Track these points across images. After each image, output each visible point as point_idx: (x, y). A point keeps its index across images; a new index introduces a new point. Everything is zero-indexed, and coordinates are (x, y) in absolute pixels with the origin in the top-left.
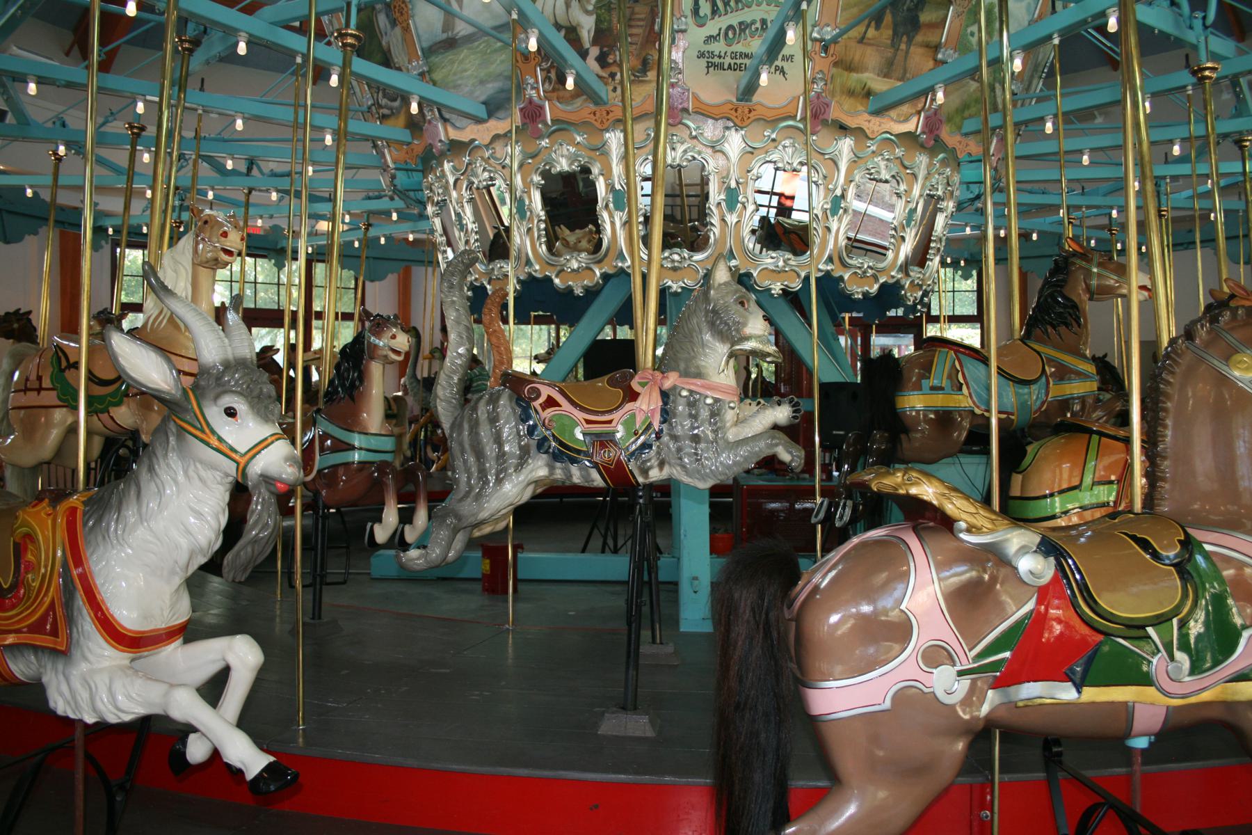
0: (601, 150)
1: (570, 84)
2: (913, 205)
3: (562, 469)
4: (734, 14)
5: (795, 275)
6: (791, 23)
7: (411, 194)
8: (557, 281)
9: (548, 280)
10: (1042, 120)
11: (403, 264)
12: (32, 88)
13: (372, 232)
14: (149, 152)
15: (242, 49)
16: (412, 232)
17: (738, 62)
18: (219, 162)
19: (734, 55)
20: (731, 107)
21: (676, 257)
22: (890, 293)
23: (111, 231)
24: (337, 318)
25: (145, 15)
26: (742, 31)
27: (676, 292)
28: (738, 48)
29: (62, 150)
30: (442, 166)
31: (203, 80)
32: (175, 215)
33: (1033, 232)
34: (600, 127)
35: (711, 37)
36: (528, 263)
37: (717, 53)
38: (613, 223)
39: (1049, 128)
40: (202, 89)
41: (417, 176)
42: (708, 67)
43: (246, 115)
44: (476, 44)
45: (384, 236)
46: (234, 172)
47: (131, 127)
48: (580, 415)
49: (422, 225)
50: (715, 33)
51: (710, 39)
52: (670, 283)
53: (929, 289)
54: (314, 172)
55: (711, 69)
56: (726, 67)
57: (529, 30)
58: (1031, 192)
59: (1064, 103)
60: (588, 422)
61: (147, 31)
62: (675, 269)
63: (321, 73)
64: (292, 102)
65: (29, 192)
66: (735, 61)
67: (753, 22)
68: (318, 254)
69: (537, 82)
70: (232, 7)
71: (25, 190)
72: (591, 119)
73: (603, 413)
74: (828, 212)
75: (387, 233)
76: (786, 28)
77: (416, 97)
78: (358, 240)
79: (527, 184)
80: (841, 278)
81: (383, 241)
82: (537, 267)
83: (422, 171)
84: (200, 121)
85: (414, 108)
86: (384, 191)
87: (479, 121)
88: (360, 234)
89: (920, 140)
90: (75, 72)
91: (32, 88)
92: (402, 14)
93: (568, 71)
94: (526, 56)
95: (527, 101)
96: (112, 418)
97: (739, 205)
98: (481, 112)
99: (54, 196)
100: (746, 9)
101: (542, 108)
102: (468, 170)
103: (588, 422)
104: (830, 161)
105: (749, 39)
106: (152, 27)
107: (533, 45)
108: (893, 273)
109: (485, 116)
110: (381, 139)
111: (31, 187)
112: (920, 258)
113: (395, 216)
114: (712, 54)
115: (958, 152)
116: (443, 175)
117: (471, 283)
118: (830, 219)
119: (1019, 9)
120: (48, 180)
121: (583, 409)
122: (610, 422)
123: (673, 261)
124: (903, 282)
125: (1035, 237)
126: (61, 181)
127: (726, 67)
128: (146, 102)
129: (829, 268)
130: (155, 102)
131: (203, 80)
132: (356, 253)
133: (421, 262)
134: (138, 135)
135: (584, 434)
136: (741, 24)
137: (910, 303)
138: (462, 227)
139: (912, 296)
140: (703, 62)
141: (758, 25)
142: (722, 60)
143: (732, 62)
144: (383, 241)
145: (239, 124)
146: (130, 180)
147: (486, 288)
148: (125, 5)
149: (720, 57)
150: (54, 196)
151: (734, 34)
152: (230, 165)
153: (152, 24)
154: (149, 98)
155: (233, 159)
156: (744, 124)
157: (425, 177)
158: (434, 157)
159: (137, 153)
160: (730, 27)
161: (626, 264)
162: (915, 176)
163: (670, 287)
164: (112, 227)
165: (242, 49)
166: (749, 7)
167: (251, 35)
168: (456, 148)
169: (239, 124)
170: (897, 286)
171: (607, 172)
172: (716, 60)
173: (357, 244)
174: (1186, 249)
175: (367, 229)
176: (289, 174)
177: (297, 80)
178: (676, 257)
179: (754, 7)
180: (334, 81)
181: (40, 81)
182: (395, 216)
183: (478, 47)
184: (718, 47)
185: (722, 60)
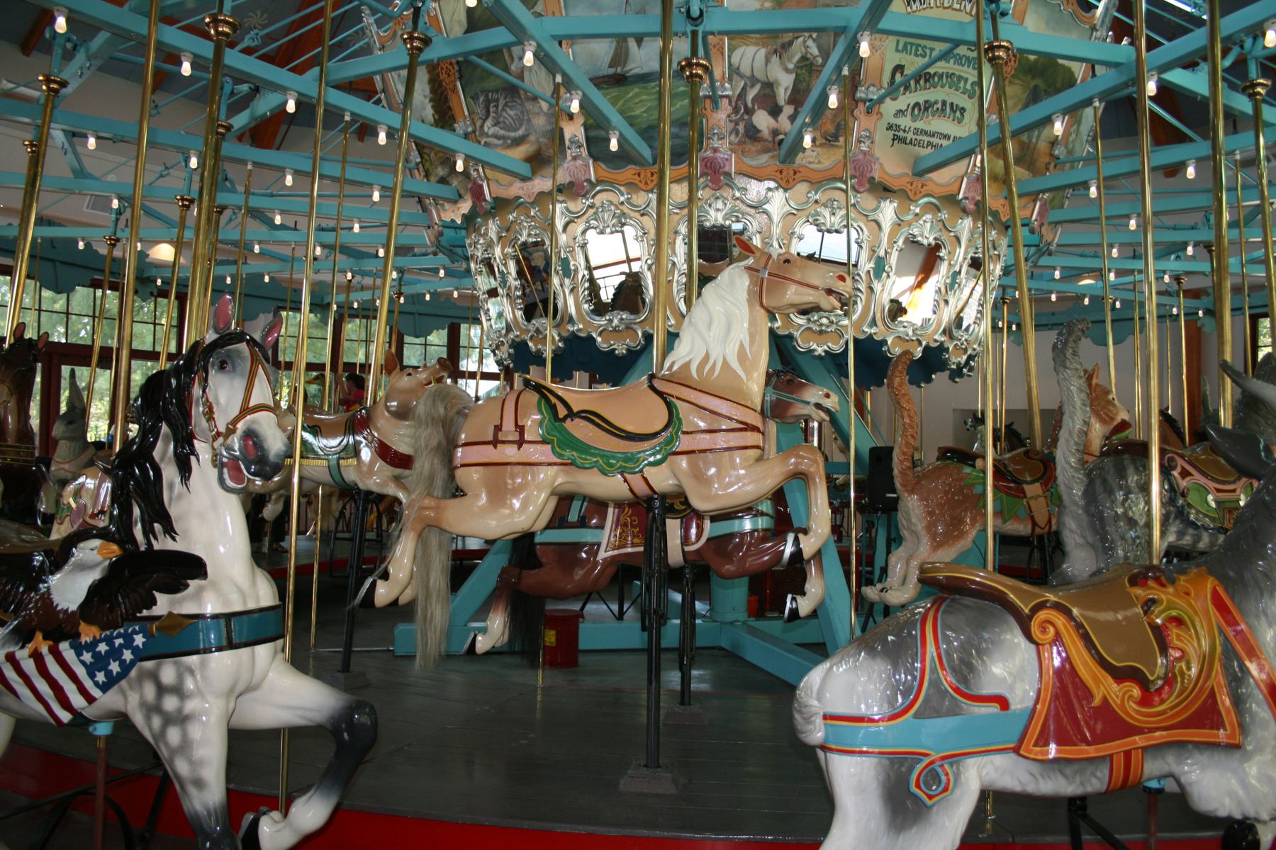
2: (957, 268)
3: (1192, 535)
4: (922, 92)
10: (1085, 185)
12: (92, 142)
17: (919, 138)
19: (916, 132)
21: (824, 321)
23: (159, 282)
25: (198, 74)
26: (926, 109)
27: (820, 355)
28: (920, 125)
30: (487, 224)
35: (900, 111)
36: (571, 320)
37: (902, 127)
38: (961, 266)
39: (1093, 191)
41: (463, 232)
42: (894, 140)
48: (1212, 485)
49: (466, 282)
50: (904, 108)
51: (900, 113)
52: (815, 346)
53: (974, 353)
55: (896, 142)
56: (908, 141)
58: (1081, 256)
59: (1109, 169)
60: (1218, 491)
62: (821, 332)
63: (366, 130)
64: (340, 158)
65: (81, 245)
66: (915, 137)
67: (936, 102)
68: (363, 309)
73: (1229, 483)
76: (828, 92)
80: (884, 342)
81: (428, 297)
84: (250, 176)
85: (460, 166)
86: (426, 246)
87: (524, 179)
89: (962, 205)
91: (92, 142)
96: (645, 479)
97: (885, 274)
98: (525, 169)
100: (932, 89)
103: (1218, 491)
104: (874, 224)
105: (930, 117)
109: (530, 175)
110: (428, 197)
114: (898, 127)
115: (1002, 215)
117: (513, 340)
119: (228, 5)
121: (1214, 480)
122: (1234, 491)
123: (822, 325)
124: (946, 345)
125: (1086, 301)
127: (908, 141)
129: (873, 331)
135: (1217, 502)
136: (926, 102)
140: (891, 133)
141: (939, 106)
142: (905, 135)
143: (914, 137)
144: (428, 297)
145: (289, 180)
147: (594, 340)
148: (180, 65)
149: (904, 131)
151: (920, 110)
160: (917, 104)
161: (776, 325)
162: (958, 240)
163: (814, 350)
164: (162, 278)
166: (935, 87)
167: (300, 94)
168: (501, 205)
169: (289, 180)
170: (942, 348)
172: (901, 134)
174: (1050, 329)
176: (333, 230)
177: (345, 138)
178: (824, 321)
179: (939, 88)
182: (442, 273)
184: (904, 122)
185: (905, 135)
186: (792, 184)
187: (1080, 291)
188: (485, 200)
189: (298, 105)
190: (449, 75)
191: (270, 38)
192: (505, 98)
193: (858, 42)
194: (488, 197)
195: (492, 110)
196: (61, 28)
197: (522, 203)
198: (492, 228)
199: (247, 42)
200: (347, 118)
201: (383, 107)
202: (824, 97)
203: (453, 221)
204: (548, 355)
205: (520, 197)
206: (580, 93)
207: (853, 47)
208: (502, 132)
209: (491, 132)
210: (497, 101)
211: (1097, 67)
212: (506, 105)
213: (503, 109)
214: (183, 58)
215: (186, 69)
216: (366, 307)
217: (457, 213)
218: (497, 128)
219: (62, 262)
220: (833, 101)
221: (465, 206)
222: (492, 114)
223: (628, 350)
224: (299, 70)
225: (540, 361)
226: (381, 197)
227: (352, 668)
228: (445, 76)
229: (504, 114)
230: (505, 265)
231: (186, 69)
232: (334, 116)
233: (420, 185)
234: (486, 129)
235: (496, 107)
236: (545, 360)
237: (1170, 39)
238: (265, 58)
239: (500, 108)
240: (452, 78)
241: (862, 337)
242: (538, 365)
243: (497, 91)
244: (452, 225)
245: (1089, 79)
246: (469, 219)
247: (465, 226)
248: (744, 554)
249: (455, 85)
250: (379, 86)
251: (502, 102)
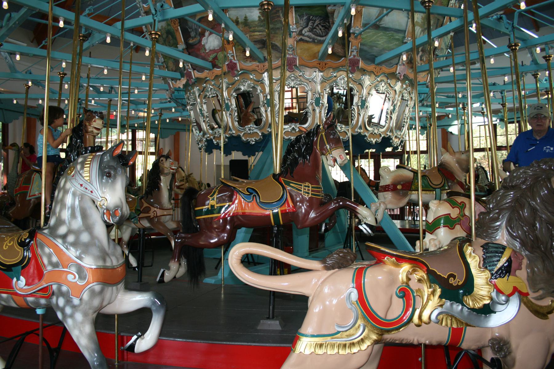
0: (261, 82)
1: (248, 54)
5: (345, 133)
6: (354, 5)
7: (179, 101)
8: (243, 138)
9: (239, 137)
11: (176, 131)
12: (18, 57)
13: (163, 117)
14: (68, 84)
15: (108, 40)
16: (181, 117)
18: (97, 88)
20: (318, 62)
22: (387, 141)
24: (144, 152)
25: (67, 26)
29: (30, 84)
31: (90, 52)
32: (78, 111)
33: (450, 114)
34: (260, 72)
36: (230, 129)
40: (90, 57)
41: (182, 93)
43: (109, 68)
44: (388, 32)
45: (169, 119)
46: (104, 92)
47: (60, 74)
49: (185, 113)
54: (138, 92)
57: (230, 32)
61: (66, 32)
63: (139, 49)
65: (15, 102)
69: (233, 53)
70: (101, 22)
71: (13, 101)
72: (374, 70)
74: (360, 107)
75: (170, 117)
77: (182, 60)
78: (157, 120)
79: (230, 95)
81: (168, 121)
82: (234, 132)
83: (185, 91)
85: (181, 65)
88: (158, 118)
90: (37, 51)
91: (18, 57)
92: (175, 24)
93: (247, 48)
94: (228, 41)
95: (229, 61)
99: (26, 102)
101: (236, 64)
102: (204, 90)
106: (68, 31)
107: (231, 38)
108: (356, 130)
111: (16, 99)
112: (399, 127)
113: (173, 110)
116: (194, 93)
118: (361, 111)
120: (24, 96)
126: (29, 96)
128: (66, 63)
130: (490, 77)
131: (90, 52)
132: (157, 127)
133: (185, 130)
134: (63, 77)
137: (395, 146)
138: (203, 115)
139: (396, 142)
144: (168, 121)
146: (60, 95)
148: (59, 22)
150: (26, 102)
152: (102, 89)
153: (67, 30)
154: (68, 61)
155: (103, 87)
156: (323, 70)
157: (186, 93)
158: (190, 85)
159: (63, 85)
165: (108, 40)
168: (199, 81)
170: (389, 139)
171: (263, 91)
173: (156, 122)
175: (161, 116)
180: (147, 53)
181: (21, 54)
183: (388, 34)
186: (324, 69)
187: (447, 112)
188: (192, 78)
189: (111, 38)
190: (175, 24)
191: (96, 10)
192: (320, 21)
193: (351, 9)
194: (194, 78)
195: (310, 24)
196: (5, 7)
197: (208, 80)
198: (196, 89)
199: (87, 12)
200: (132, 45)
201: (146, 38)
202: (336, 32)
203: (179, 87)
204: (222, 145)
205: (207, 77)
206: (233, 32)
207: (349, 10)
208: (313, 36)
209: (307, 34)
210: (315, 21)
211: (452, 18)
212: (320, 24)
213: (317, 25)
214: (60, 19)
215: (61, 24)
216: (140, 126)
217: (181, 83)
218: (311, 34)
219: (6, 110)
220: (340, 34)
221: (184, 81)
222: (309, 26)
223: (256, 141)
224: (110, 24)
225: (218, 147)
226: (146, 78)
227: (142, 280)
228: (173, 24)
229: (317, 28)
230: (230, 100)
231: (61, 24)
232: (127, 43)
233: (166, 73)
234: (303, 32)
235: (314, 23)
236: (220, 147)
237: (484, 5)
238: (93, 18)
239: (315, 25)
240: (176, 25)
241: (356, 134)
242: (217, 149)
243: (316, 16)
244: (178, 90)
245: (448, 23)
246: (186, 86)
247: (184, 90)
248: (411, 208)
249: (178, 28)
250: (145, 30)
251: (317, 22)
